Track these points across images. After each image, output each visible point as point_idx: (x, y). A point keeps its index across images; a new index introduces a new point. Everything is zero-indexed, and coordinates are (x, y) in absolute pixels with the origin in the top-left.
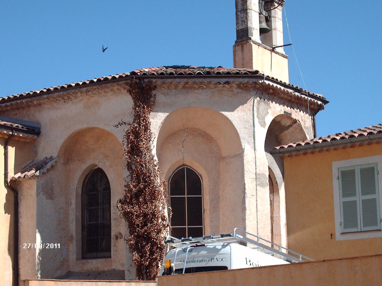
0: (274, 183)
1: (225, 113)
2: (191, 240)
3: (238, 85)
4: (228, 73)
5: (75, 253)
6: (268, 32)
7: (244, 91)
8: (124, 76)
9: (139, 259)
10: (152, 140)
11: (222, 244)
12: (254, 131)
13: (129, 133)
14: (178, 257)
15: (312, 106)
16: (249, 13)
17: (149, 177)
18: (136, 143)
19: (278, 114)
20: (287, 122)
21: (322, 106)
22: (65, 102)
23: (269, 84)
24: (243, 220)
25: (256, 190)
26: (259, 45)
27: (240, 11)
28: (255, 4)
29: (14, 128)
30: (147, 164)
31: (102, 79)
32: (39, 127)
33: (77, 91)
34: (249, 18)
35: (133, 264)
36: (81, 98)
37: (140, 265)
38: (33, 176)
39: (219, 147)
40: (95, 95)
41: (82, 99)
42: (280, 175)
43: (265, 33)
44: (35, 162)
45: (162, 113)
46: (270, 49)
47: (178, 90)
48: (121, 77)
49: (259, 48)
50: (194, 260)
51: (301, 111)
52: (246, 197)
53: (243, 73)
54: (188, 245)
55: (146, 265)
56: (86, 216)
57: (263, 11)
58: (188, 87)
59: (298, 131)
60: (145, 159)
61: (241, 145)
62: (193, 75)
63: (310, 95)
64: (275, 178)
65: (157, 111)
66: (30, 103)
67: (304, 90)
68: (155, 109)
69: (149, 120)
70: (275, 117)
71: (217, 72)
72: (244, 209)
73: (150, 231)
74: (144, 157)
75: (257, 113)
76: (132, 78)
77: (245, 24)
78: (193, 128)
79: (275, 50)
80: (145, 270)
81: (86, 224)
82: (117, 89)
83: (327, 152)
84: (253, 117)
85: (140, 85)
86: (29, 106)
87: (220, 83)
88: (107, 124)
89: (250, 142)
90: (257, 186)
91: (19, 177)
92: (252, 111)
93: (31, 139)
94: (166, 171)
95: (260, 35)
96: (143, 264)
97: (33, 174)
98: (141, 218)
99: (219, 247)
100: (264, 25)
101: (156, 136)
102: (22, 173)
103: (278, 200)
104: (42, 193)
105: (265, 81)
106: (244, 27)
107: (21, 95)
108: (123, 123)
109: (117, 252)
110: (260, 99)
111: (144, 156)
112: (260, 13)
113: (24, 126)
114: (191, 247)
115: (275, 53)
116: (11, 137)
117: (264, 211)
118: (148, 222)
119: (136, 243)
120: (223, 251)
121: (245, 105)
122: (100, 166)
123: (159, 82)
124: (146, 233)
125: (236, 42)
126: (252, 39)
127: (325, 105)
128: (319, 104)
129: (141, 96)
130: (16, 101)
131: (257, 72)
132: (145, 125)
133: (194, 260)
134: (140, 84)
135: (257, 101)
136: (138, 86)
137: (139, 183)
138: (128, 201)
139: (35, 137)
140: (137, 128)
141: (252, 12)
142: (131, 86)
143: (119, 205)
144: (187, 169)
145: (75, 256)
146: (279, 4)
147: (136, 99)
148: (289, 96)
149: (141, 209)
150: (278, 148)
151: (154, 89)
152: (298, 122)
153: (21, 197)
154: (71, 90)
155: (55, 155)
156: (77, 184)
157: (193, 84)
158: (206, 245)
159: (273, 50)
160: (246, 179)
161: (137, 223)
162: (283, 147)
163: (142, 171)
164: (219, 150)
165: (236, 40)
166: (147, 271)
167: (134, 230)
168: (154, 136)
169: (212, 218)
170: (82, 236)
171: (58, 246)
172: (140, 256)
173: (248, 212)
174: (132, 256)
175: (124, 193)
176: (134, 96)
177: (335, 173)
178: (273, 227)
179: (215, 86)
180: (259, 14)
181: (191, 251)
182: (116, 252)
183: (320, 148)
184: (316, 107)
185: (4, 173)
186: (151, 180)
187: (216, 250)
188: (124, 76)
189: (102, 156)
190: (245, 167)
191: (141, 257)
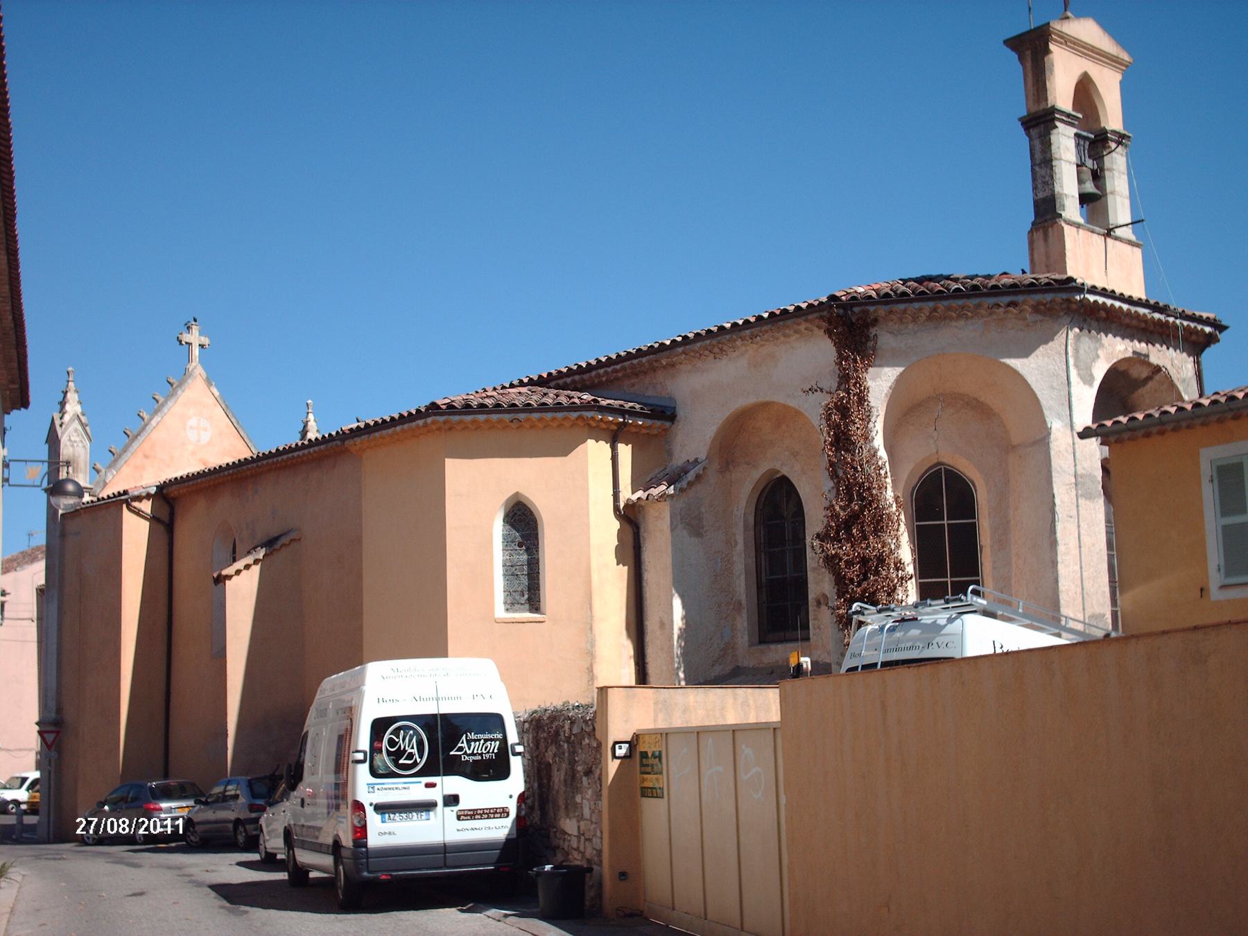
3: (1033, 305)
4: (1014, 286)
5: (746, 632)
7: (1047, 318)
10: (873, 420)
11: (948, 616)
12: (1069, 394)
13: (829, 408)
14: (869, 642)
17: (869, 489)
19: (1119, 358)
26: (1078, 226)
28: (1067, 149)
30: (865, 466)
31: (778, 312)
33: (734, 337)
34: (1057, 177)
36: (743, 349)
38: (663, 496)
40: (767, 343)
41: (747, 351)
47: (919, 323)
49: (1078, 231)
57: (1087, 159)
61: (1044, 422)
62: (945, 293)
65: (880, 366)
66: (655, 364)
67: (1172, 307)
68: (877, 362)
69: (865, 383)
72: (1054, 543)
74: (859, 453)
79: (1112, 233)
81: (764, 580)
82: (806, 329)
86: (654, 370)
87: (998, 306)
91: (639, 498)
92: (1064, 356)
93: (659, 428)
99: (942, 622)
100: (1090, 187)
101: (880, 411)
104: (680, 526)
105: (1088, 296)
107: (639, 350)
109: (819, 628)
110: (1081, 330)
112: (1080, 163)
113: (645, 405)
114: (893, 622)
117: (1093, 545)
120: (950, 628)
121: (1051, 344)
122: (785, 471)
123: (882, 310)
125: (1033, 224)
127: (1220, 333)
131: (1071, 280)
137: (851, 501)
139: (668, 424)
142: (830, 323)
145: (746, 638)
147: (839, 346)
152: (1164, 370)
154: (724, 337)
155: (702, 456)
156: (746, 507)
158: (919, 618)
159: (1109, 233)
162: (1104, 425)
163: (855, 479)
165: (1034, 219)
170: (758, 600)
173: (1061, 548)
175: (825, 520)
176: (837, 340)
177: (1206, 469)
179: (989, 311)
180: (1078, 166)
182: (818, 630)
184: (1201, 339)
187: (936, 628)
188: (816, 303)
189: (787, 453)
190: (1053, 464)
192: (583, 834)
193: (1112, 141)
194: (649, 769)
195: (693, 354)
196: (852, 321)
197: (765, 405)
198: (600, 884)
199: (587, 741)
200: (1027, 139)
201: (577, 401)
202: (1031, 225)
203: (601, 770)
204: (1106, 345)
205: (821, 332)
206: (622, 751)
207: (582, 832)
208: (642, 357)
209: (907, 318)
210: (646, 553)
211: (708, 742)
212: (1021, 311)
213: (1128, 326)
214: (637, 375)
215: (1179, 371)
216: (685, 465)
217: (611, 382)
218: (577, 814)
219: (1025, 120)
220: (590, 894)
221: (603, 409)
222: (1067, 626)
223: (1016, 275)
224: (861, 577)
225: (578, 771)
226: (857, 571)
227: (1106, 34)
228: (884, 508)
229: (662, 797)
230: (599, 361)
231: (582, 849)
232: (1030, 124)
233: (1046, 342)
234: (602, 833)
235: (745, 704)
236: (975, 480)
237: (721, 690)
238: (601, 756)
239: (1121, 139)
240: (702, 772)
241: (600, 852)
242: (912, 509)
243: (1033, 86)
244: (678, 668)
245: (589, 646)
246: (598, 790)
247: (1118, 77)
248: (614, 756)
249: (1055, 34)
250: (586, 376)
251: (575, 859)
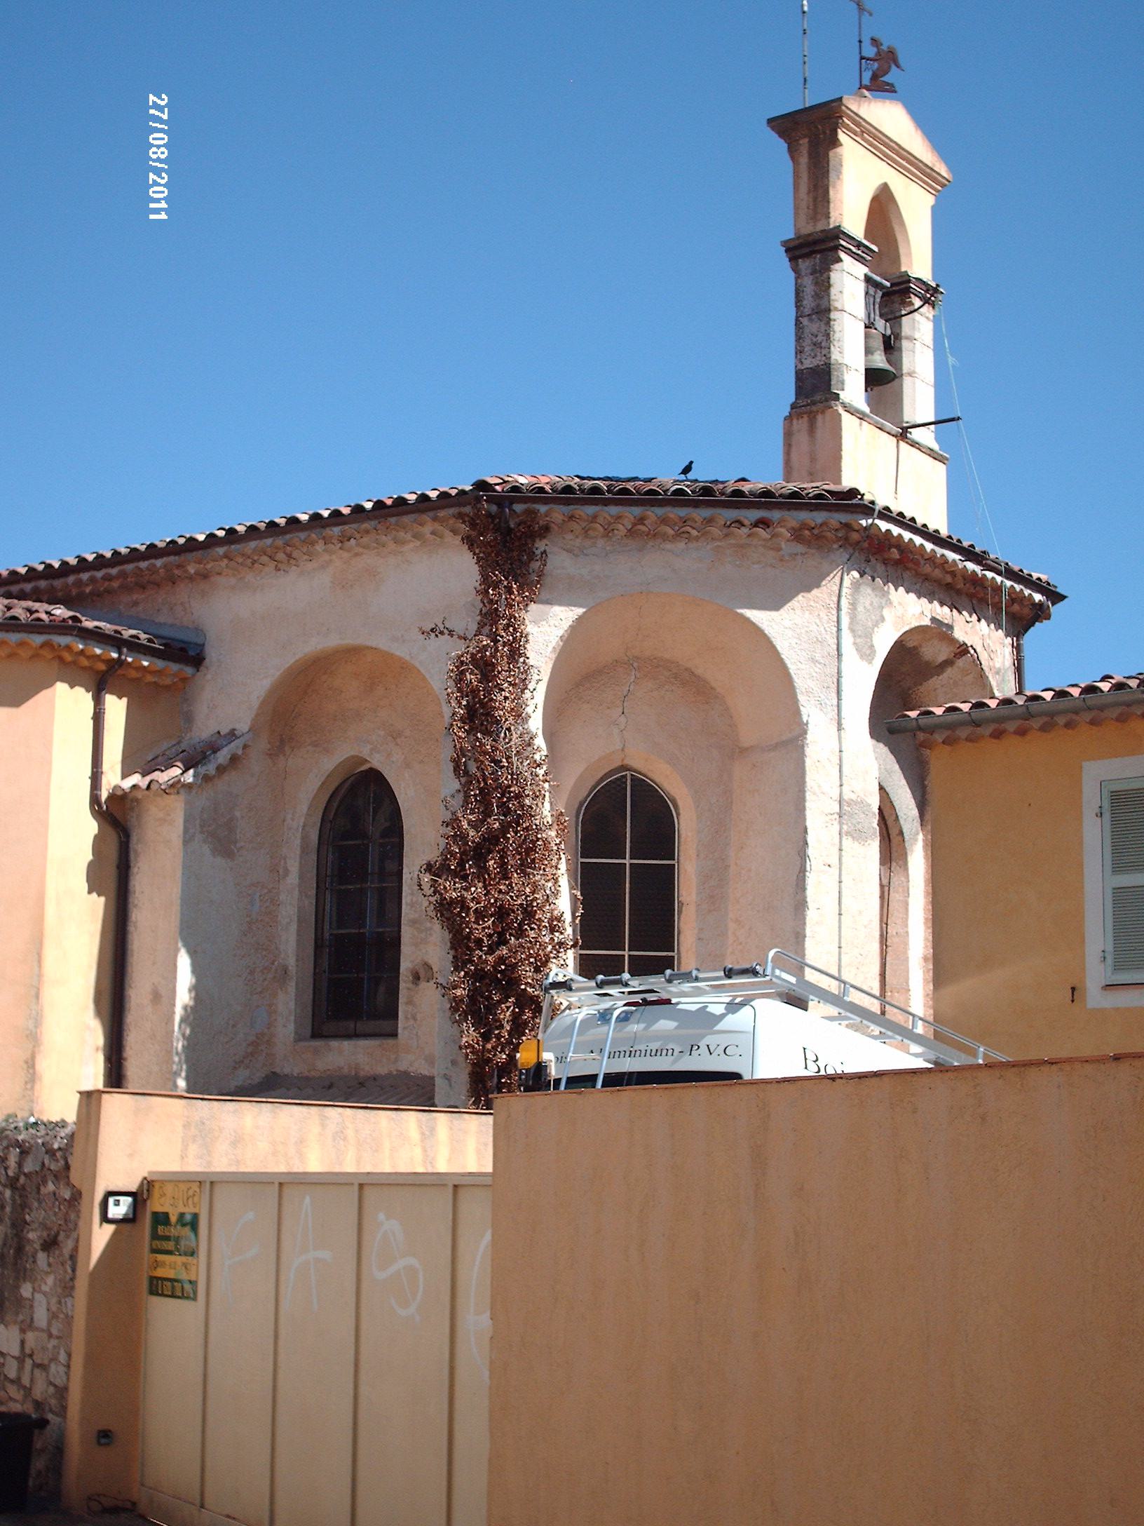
0: (893, 832)
1: (754, 615)
2: (626, 985)
3: (793, 528)
4: (767, 493)
5: (292, 1018)
6: (889, 382)
7: (813, 551)
8: (453, 492)
9: (478, 1044)
10: (531, 686)
11: (728, 1000)
12: (839, 673)
13: (462, 663)
14: (582, 1038)
15: (1016, 607)
16: (835, 320)
17: (518, 796)
18: (484, 695)
19: (913, 626)
20: (940, 651)
21: (1046, 607)
22: (279, 570)
23: (888, 531)
24: (797, 938)
25: (841, 850)
26: (862, 417)
27: (809, 315)
29: (126, 641)
30: (514, 759)
31: (389, 502)
32: (200, 641)
35: (461, 1059)
36: (326, 557)
37: (481, 1062)
38: (176, 786)
39: (731, 717)
40: (365, 551)
42: (911, 810)
43: (881, 385)
44: (183, 746)
45: (563, 608)
46: (893, 433)
47: (614, 539)
48: (444, 495)
49: (861, 425)
50: (635, 1048)
51: (983, 621)
52: (808, 868)
53: (810, 495)
54: (617, 1000)
55: (498, 1062)
56: (328, 908)
58: (643, 532)
59: (970, 678)
60: (508, 743)
61: (798, 713)
62: (661, 494)
63: (1010, 574)
64: (897, 817)
65: (549, 602)
66: (176, 572)
67: (992, 556)
68: (544, 595)
69: (523, 627)
70: (904, 633)
71: (734, 491)
72: (800, 905)
73: (515, 959)
74: (504, 739)
75: (851, 618)
76: (479, 499)
77: (823, 353)
78: (655, 659)
79: (908, 435)
80: (495, 1080)
81: (327, 935)
82: (433, 533)
83: (1070, 732)
84: (839, 630)
85: (499, 522)
86: (173, 581)
87: (740, 524)
88: (400, 635)
89: (826, 704)
90: (844, 838)
92: (834, 612)
93: (175, 675)
94: (569, 783)
95: (866, 391)
96: (490, 1060)
97: (176, 779)
98: (489, 920)
99: (718, 1010)
100: (880, 361)
102: (144, 776)
103: (905, 884)
105: (877, 522)
106: (818, 361)
108: (445, 631)
109: (415, 1019)
110: (861, 576)
111: (505, 734)
114: (625, 1005)
115: (907, 443)
116: (116, 667)
118: (511, 934)
119: (473, 996)
120: (731, 1021)
121: (815, 592)
122: (377, 762)
123: (558, 513)
124: (503, 967)
125: (793, 406)
126: (841, 397)
127: (1053, 605)
128: (1037, 601)
129: (503, 554)
130: (136, 564)
131: (853, 493)
132: (513, 642)
133: (635, 1048)
134: (500, 518)
135: (850, 582)
136: (495, 525)
137: (487, 813)
138: (453, 867)
139: (189, 670)
140: (487, 651)
141: (842, 277)
142: (473, 525)
143: (426, 878)
144: (634, 779)
145: (291, 1027)
146: (926, 301)
148: (947, 572)
149: (491, 894)
150: (913, 714)
151: (542, 537)
152: (972, 652)
153: (139, 847)
154: (297, 534)
155: (243, 726)
156: (307, 814)
157: (661, 523)
158: (674, 1001)
159: (903, 435)
160: (808, 813)
161: (476, 934)
162: (931, 713)
164: (730, 726)
165: (794, 400)
166: (503, 1081)
167: (467, 955)
168: (535, 677)
169: (702, 929)
170: (315, 968)
172: (483, 1035)
173: (811, 916)
174: (459, 1035)
177: (1091, 797)
178: (887, 965)
179: (725, 531)
180: (866, 327)
181: (625, 1018)
182: (412, 1022)
183: (1045, 719)
184: (1026, 611)
185: (89, 774)
186: (522, 806)
187: (706, 1020)
188: (453, 492)
189: (382, 733)
190: (808, 779)
191: (486, 1037)
192: (31, 1356)
193: (916, 295)
194: (170, 1245)
195: (240, 560)
196: (509, 526)
197: (353, 652)
198: (59, 1450)
199: (51, 1187)
200: (792, 275)
201: (44, 616)
202: (788, 409)
203: (77, 1241)
204: (895, 603)
205: (457, 540)
206: (119, 1209)
207: (28, 1351)
208: (156, 558)
209: (595, 529)
210: (137, 877)
211: (304, 1206)
212: (774, 536)
213: (926, 578)
214: (143, 587)
215: (992, 656)
216: (214, 739)
217: (99, 595)
218: (21, 1317)
219: (791, 245)
220: (39, 1463)
221: (86, 634)
222: (915, 1030)
223: (758, 483)
224: (495, 938)
225: (29, 1240)
226: (489, 928)
227: (919, 132)
228: (539, 830)
229: (195, 1299)
230: (82, 560)
231: (26, 1381)
232: (797, 253)
233: (808, 589)
234: (69, 1355)
235: (340, 1135)
236: (677, 798)
237: (300, 1108)
238: (78, 1217)
239: (930, 294)
240: (284, 1259)
241: (62, 1392)
242: (577, 836)
243: (809, 192)
244: (177, 1074)
245: (31, 1024)
246: (68, 1277)
247: (930, 200)
248: (105, 1219)
249: (849, 118)
250: (58, 583)
251: (11, 1399)
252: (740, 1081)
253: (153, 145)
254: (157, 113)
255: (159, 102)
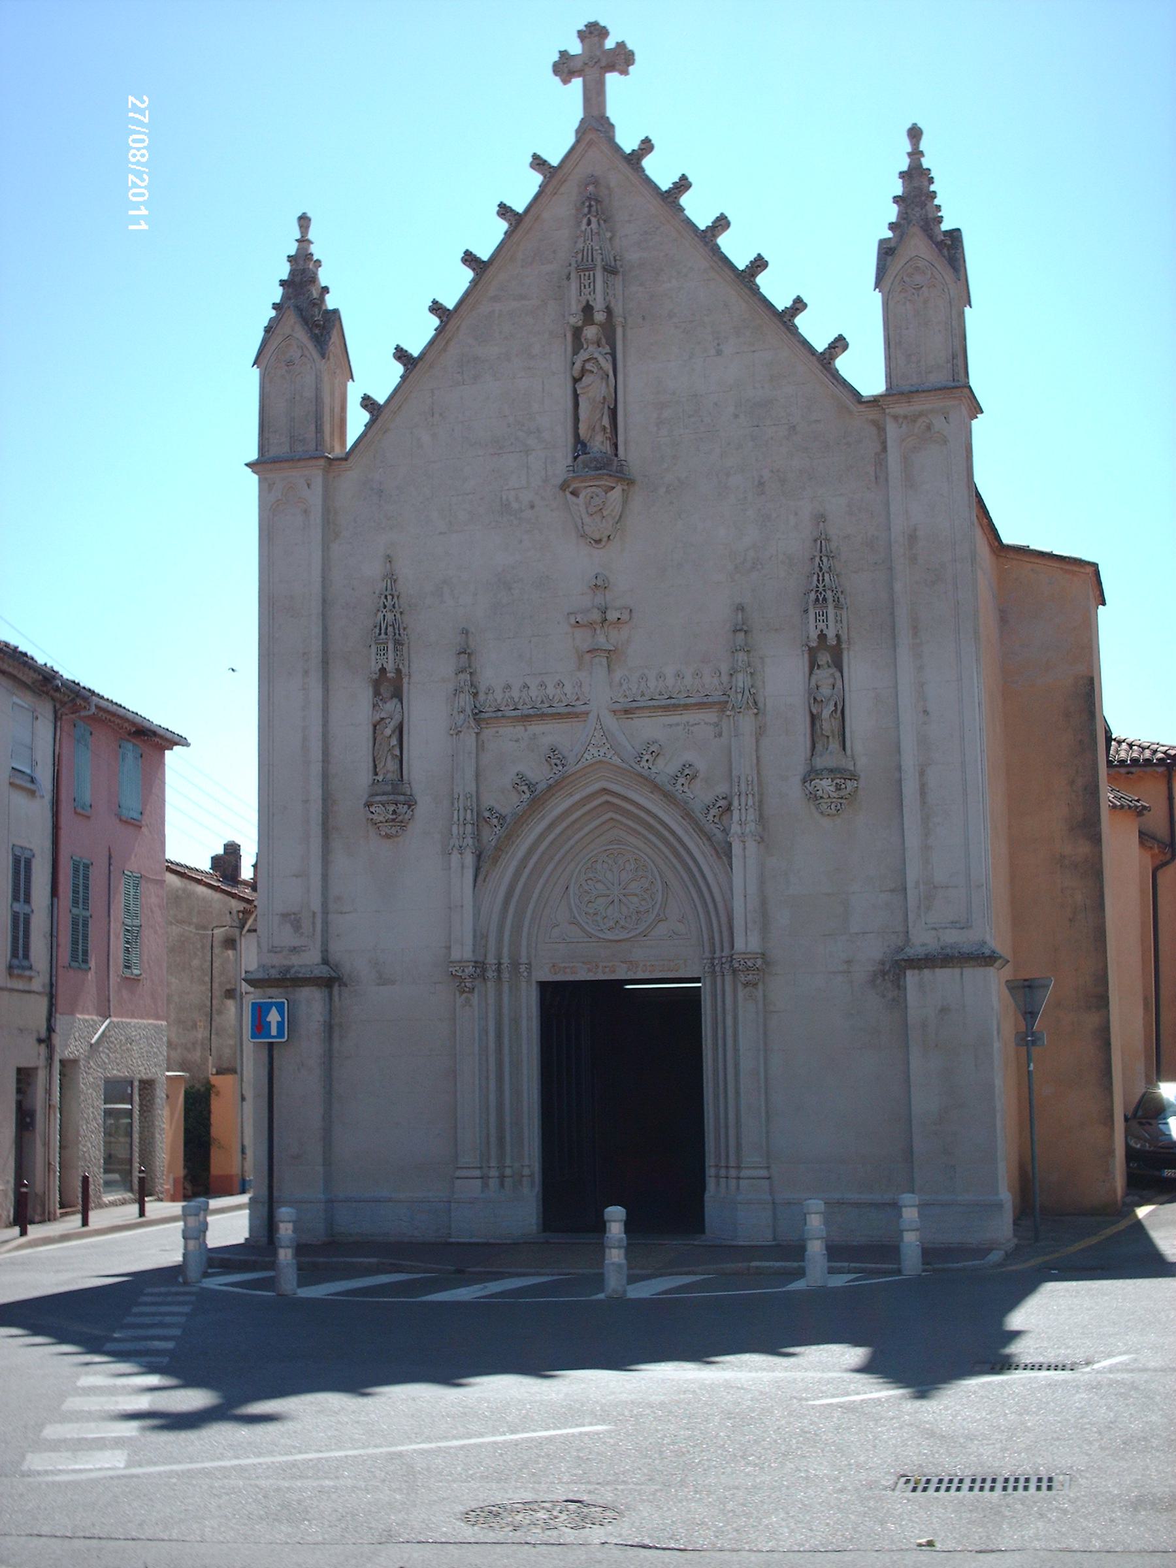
171: (136, 220)
252: (933, 1548)
253: (145, 187)
254: (137, 116)
255: (138, 103)
